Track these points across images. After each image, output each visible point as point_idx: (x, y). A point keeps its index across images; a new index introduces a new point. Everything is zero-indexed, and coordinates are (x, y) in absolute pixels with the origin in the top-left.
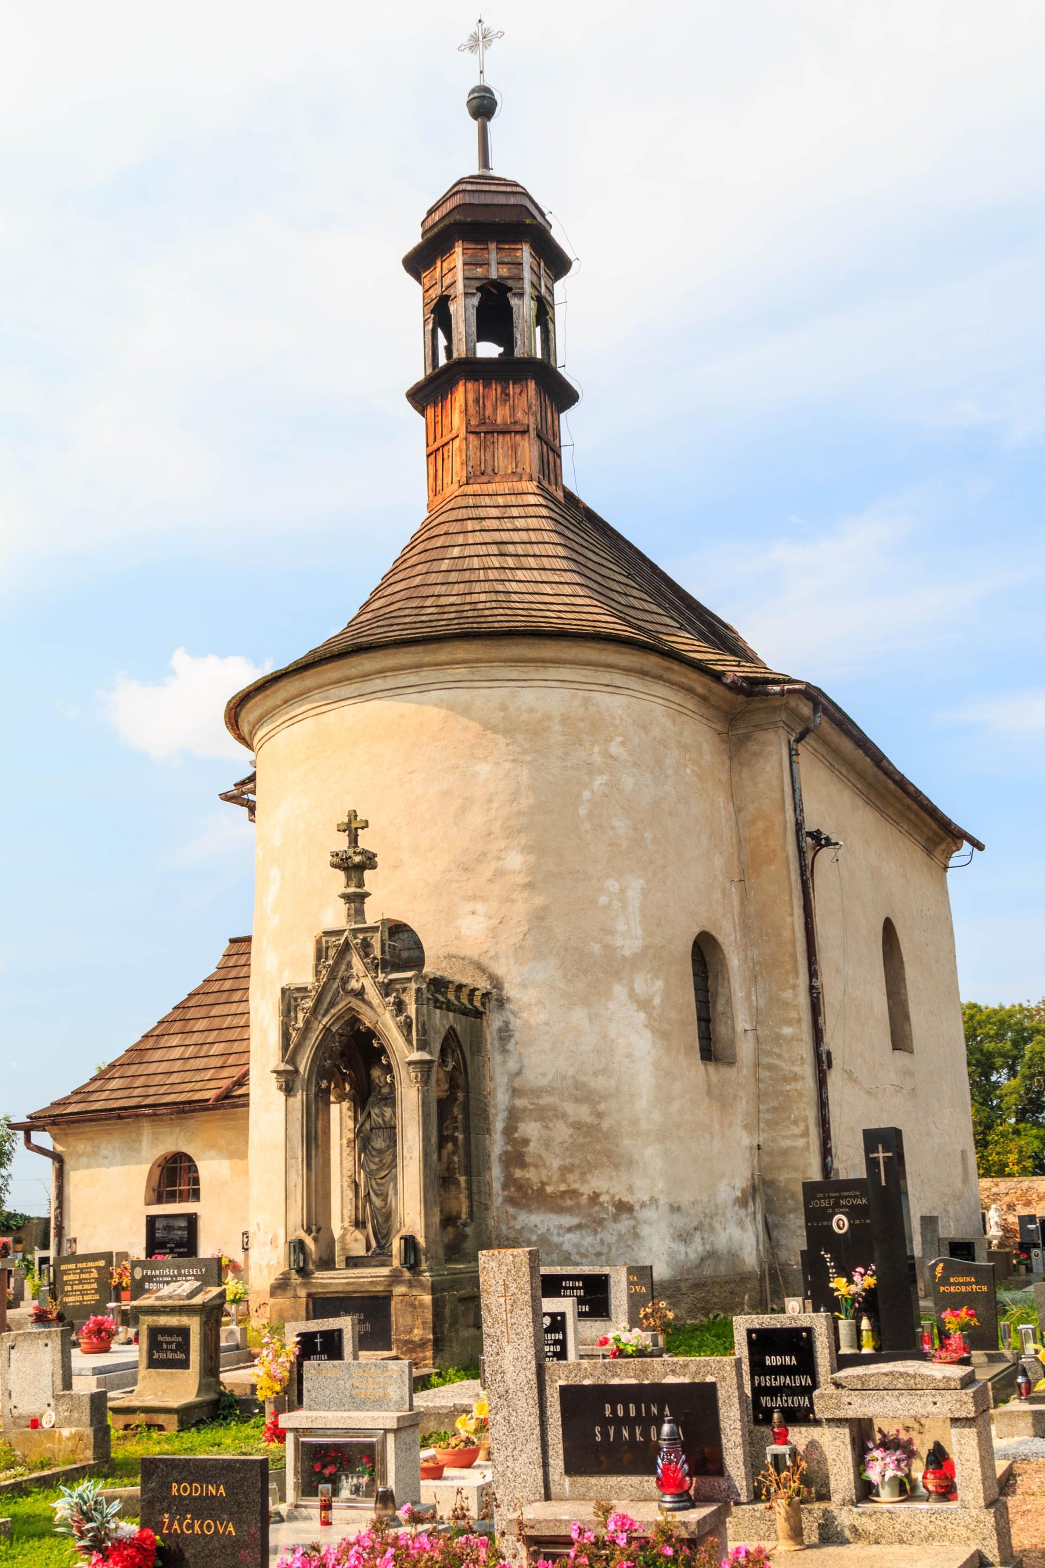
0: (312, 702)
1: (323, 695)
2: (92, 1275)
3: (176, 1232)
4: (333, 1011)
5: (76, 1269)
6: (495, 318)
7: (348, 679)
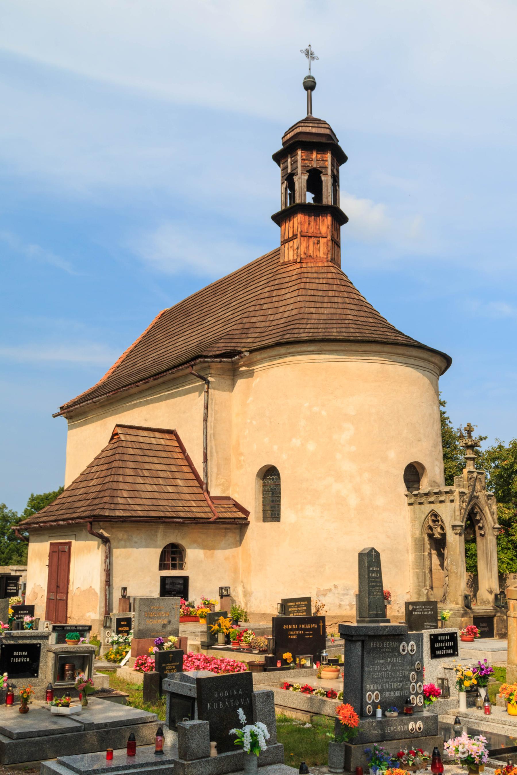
0: (381, 357)
1: (388, 356)
2: (303, 608)
3: (177, 586)
4: (471, 503)
5: (295, 605)
6: (314, 183)
7: (403, 355)
